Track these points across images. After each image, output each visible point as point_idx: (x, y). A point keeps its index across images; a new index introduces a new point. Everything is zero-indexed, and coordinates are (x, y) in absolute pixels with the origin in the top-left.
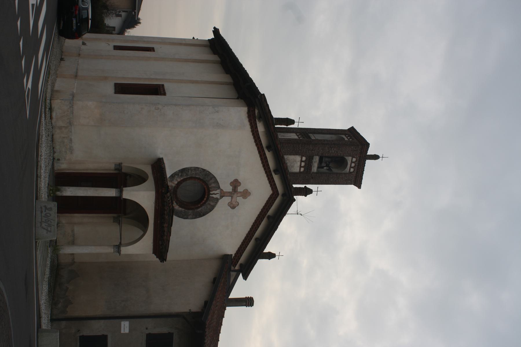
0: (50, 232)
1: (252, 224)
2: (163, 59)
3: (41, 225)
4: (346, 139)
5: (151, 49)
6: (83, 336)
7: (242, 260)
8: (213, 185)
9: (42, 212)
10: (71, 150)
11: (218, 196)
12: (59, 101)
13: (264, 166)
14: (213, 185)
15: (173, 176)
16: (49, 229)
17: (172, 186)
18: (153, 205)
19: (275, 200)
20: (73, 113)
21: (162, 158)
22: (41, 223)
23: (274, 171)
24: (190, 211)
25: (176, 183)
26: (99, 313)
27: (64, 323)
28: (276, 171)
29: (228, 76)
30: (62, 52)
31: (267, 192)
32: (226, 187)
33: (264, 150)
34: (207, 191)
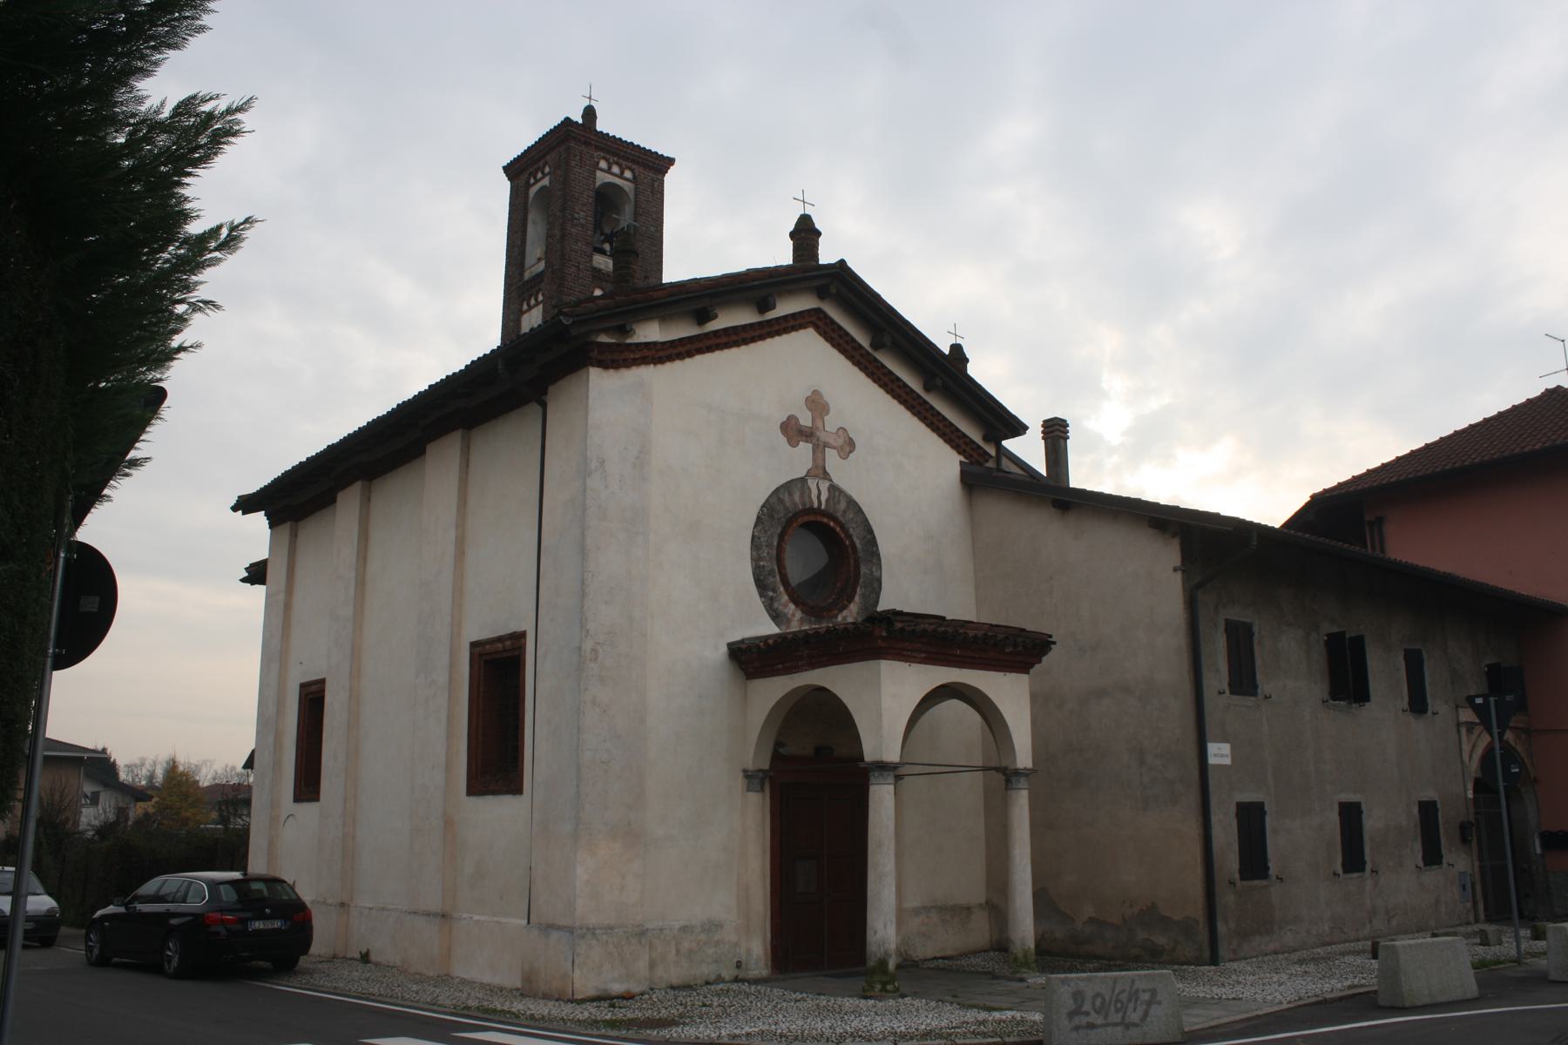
0: (1154, 992)
1: (889, 398)
2: (356, 653)
3: (1136, 1025)
4: (546, 182)
5: (313, 699)
6: (1241, 872)
7: (974, 434)
8: (797, 497)
9: (1091, 1026)
10: (712, 926)
11: (824, 486)
12: (577, 972)
13: (746, 342)
14: (797, 497)
15: (776, 617)
16: (1146, 996)
17: (802, 621)
18: (916, 667)
19: (833, 322)
20: (611, 928)
21: (730, 645)
22: (1128, 1026)
23: (762, 311)
24: (863, 570)
25: (792, 606)
26: (1193, 829)
27: (1221, 928)
28: (764, 306)
29: (433, 450)
30: (335, 957)
31: (808, 342)
32: (798, 460)
33: (706, 336)
34: (811, 518)
